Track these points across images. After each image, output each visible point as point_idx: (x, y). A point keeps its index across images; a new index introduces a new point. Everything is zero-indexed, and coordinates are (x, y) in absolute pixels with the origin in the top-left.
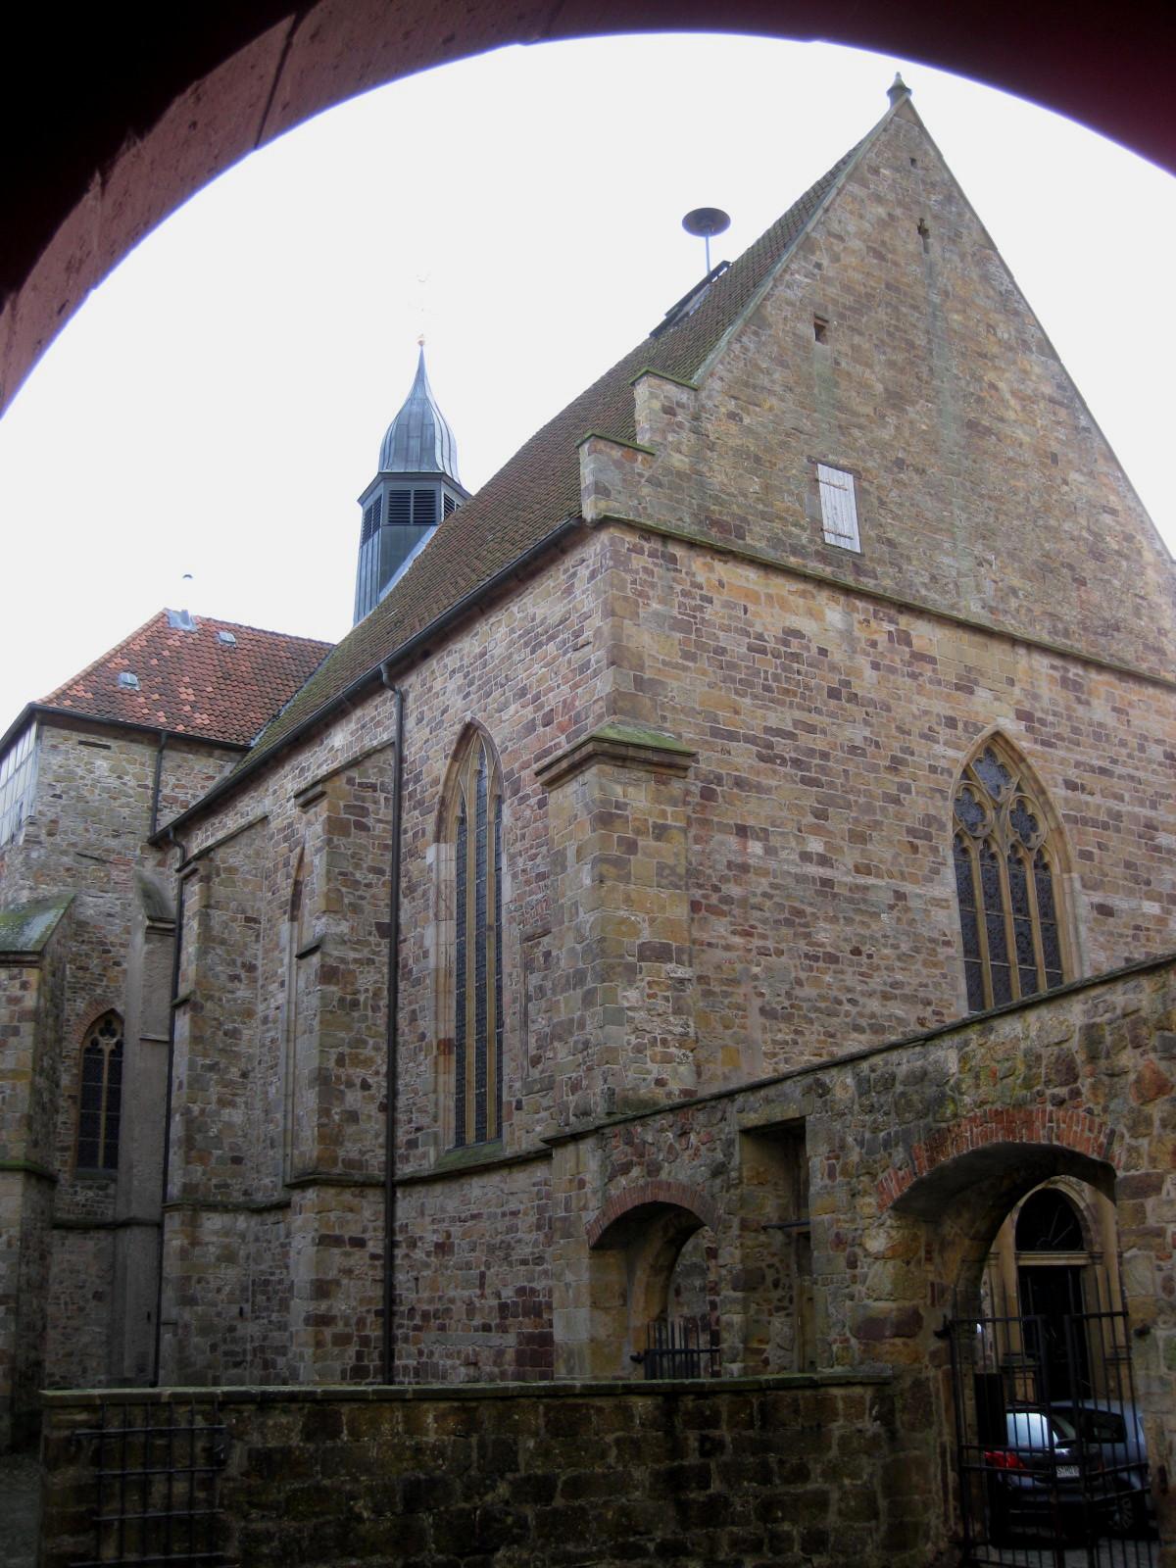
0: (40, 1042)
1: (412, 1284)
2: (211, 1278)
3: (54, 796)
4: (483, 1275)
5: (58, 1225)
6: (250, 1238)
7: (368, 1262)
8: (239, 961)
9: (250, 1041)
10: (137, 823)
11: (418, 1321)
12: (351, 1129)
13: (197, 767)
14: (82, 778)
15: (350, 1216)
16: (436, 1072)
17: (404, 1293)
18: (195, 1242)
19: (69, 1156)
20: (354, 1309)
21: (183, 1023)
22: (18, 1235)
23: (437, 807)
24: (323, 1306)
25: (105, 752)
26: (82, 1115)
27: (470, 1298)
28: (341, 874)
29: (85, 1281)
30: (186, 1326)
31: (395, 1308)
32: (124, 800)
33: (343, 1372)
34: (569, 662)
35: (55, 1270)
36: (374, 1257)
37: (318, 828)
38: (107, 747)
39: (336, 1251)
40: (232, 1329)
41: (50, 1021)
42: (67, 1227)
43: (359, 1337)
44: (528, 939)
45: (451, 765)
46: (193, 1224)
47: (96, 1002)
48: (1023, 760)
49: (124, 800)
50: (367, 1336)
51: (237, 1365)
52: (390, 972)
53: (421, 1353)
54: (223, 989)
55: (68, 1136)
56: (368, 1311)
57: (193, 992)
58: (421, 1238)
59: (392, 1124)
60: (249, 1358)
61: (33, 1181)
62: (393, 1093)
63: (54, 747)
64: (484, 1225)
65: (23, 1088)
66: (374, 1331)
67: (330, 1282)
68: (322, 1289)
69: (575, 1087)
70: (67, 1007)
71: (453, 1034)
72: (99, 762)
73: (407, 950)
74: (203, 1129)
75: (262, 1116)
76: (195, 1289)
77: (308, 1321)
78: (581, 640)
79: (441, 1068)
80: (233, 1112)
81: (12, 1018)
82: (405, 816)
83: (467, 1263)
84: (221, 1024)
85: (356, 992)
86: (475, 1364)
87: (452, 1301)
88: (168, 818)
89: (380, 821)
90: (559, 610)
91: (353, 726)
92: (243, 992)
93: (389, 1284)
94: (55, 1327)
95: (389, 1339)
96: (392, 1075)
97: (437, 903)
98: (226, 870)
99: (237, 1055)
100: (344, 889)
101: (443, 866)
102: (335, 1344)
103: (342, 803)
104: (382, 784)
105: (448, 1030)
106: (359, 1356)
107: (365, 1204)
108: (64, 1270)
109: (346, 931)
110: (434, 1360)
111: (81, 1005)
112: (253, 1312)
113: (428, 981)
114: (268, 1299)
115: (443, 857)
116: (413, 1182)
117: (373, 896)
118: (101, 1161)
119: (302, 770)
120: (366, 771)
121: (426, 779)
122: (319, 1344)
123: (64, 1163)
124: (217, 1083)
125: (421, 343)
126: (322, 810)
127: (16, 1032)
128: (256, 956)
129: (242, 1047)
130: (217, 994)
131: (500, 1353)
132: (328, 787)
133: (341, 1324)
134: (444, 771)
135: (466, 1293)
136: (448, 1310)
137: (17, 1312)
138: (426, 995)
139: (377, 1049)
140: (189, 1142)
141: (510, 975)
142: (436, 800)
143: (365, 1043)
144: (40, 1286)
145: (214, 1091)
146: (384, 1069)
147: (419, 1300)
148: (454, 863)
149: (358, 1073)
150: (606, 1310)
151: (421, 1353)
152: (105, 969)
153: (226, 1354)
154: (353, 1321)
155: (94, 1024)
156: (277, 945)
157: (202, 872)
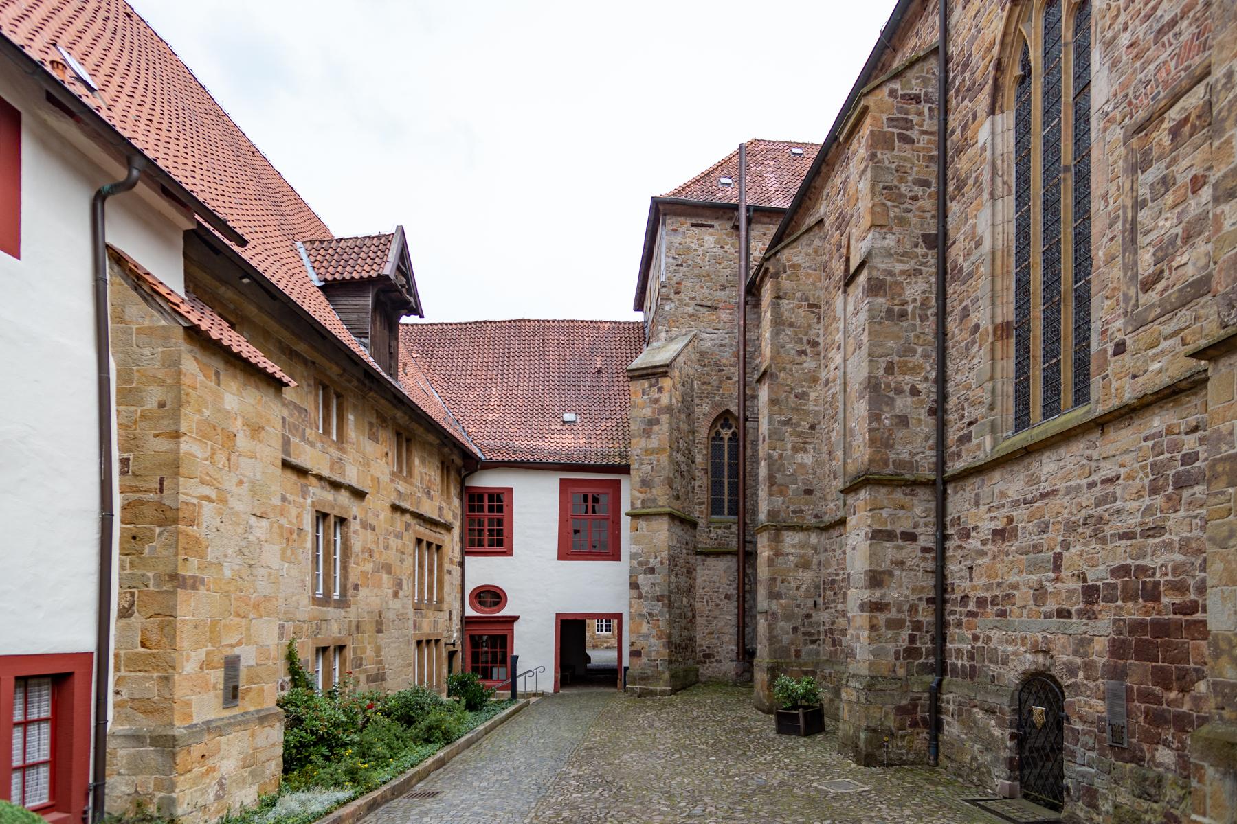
1: (966, 573)
2: (791, 579)
4: (1058, 558)
6: (821, 549)
7: (920, 554)
9: (816, 401)
11: (972, 607)
12: (901, 433)
14: (696, 250)
15: (901, 512)
17: (957, 583)
18: (778, 554)
20: (907, 596)
21: (764, 393)
24: (877, 594)
25: (710, 230)
27: (1040, 583)
30: (774, 614)
31: (947, 596)
33: (897, 653)
35: (699, 581)
36: (925, 550)
38: (712, 226)
39: (888, 544)
40: (809, 616)
41: (683, 416)
42: (708, 554)
43: (911, 622)
46: (776, 540)
47: (715, 405)
50: (919, 622)
52: (937, 283)
53: (976, 638)
54: (793, 362)
55: (703, 495)
56: (920, 599)
57: (770, 366)
58: (975, 528)
59: (942, 427)
60: (822, 637)
62: (943, 397)
63: (675, 230)
64: (1054, 503)
65: (664, 459)
66: (926, 616)
67: (883, 573)
68: (876, 579)
70: (697, 410)
71: (1012, 317)
72: (706, 238)
74: (782, 468)
76: (779, 587)
77: (862, 607)
79: (998, 355)
80: (805, 456)
83: (1035, 546)
84: (792, 389)
85: (904, 303)
86: (1046, 652)
87: (1015, 586)
92: (809, 363)
93: (940, 575)
95: (942, 624)
96: (942, 380)
97: (993, 180)
98: (790, 266)
99: (807, 412)
100: (889, 203)
101: (999, 140)
103: (885, 117)
104: (926, 94)
105: (1007, 312)
106: (912, 639)
107: (916, 502)
109: (892, 244)
110: (992, 645)
111: (706, 408)
115: (999, 129)
120: (909, 82)
122: (873, 628)
123: (701, 512)
124: (791, 434)
127: (657, 422)
129: (811, 406)
130: (788, 366)
131: (1083, 643)
136: (1009, 596)
137: (670, 606)
138: (981, 286)
139: (926, 356)
140: (771, 478)
141: (1105, 197)
143: (915, 352)
144: (690, 591)
145: (789, 441)
146: (933, 375)
147: (974, 588)
149: (908, 380)
151: (976, 638)
152: (721, 382)
153: (805, 634)
154: (906, 607)
155: (715, 421)
157: (772, 270)
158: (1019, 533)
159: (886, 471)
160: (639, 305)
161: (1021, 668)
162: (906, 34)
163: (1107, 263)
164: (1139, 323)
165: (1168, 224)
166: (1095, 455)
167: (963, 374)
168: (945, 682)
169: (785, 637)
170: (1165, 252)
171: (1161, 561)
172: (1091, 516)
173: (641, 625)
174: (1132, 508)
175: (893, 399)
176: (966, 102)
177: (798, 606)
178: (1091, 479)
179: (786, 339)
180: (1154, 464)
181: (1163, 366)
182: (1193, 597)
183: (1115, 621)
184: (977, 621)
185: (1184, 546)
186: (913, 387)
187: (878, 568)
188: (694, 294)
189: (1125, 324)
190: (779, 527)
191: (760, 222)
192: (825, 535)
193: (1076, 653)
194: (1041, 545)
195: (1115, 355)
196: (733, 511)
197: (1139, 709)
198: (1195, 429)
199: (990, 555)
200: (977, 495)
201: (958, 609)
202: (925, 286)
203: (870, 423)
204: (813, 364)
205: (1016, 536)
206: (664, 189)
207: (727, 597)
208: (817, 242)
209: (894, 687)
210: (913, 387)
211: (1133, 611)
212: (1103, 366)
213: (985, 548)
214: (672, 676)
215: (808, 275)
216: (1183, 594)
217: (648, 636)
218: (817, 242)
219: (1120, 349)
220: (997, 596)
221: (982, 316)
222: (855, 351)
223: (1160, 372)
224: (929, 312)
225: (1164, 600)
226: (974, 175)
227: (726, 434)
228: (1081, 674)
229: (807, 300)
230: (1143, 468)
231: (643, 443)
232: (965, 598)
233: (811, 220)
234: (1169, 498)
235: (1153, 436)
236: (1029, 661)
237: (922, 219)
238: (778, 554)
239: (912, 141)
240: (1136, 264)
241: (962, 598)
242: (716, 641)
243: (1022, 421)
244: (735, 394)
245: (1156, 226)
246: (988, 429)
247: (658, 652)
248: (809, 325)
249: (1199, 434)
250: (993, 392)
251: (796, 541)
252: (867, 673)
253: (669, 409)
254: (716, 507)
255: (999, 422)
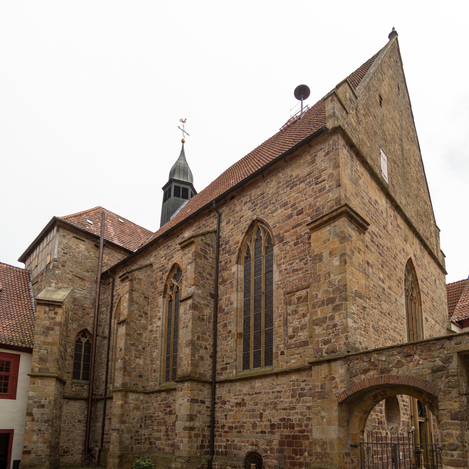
0: (62, 334)
1: (224, 417)
2: (131, 415)
3: (64, 253)
4: (261, 414)
5: (65, 398)
6: (144, 402)
8: (142, 311)
9: (145, 337)
10: (95, 269)
12: (201, 363)
13: (115, 255)
14: (74, 249)
15: (200, 392)
16: (236, 344)
17: (220, 420)
18: (126, 403)
19: (70, 375)
20: (201, 425)
22: (53, 399)
23: (237, 252)
25: (83, 242)
26: (75, 362)
28: (199, 272)
29: (75, 416)
30: (122, 431)
31: (215, 425)
32: (90, 260)
33: (197, 447)
34: (313, 189)
35: (64, 412)
36: (207, 407)
37: (190, 255)
38: (84, 241)
39: (196, 404)
41: (65, 328)
42: (70, 399)
43: (202, 435)
44: (288, 293)
45: (245, 236)
46: (125, 396)
47: (79, 326)
48: (414, 269)
49: (90, 260)
51: (139, 443)
54: (137, 319)
55: (71, 370)
56: (205, 426)
58: (228, 401)
60: (143, 441)
61: (58, 382)
62: (215, 352)
64: (260, 396)
65: (55, 349)
66: (207, 433)
67: (194, 415)
68: (191, 418)
69: (326, 342)
70: (70, 326)
71: (242, 332)
72: (81, 245)
73: (223, 303)
74: (129, 365)
75: (150, 362)
76: (125, 418)
78: (319, 180)
80: (140, 360)
81: (51, 324)
82: (220, 257)
83: (253, 410)
84: (136, 331)
86: (256, 445)
87: (245, 423)
88: (105, 269)
89: (211, 258)
90: (307, 170)
91: (194, 228)
92: (143, 321)
94: (64, 431)
96: (215, 345)
97: (237, 285)
98: (138, 279)
99: (141, 342)
100: (200, 278)
101: (239, 273)
102: (195, 437)
103: (199, 247)
105: (241, 329)
106: (202, 441)
108: (67, 413)
110: (235, 443)
111: (75, 326)
112: (145, 426)
113: (233, 313)
114: (152, 422)
115: (239, 270)
116: (223, 382)
117: (209, 283)
118: (81, 378)
119: (169, 247)
121: (231, 243)
122: (190, 437)
123: (68, 377)
125: (183, 142)
126: (193, 248)
128: (148, 310)
129: (143, 340)
130: (135, 320)
131: (270, 442)
132: (195, 240)
133: (197, 430)
134: (242, 238)
135: (252, 420)
136: (242, 426)
137: (52, 426)
138: (232, 317)
140: (124, 369)
141: (278, 307)
142: (237, 249)
143: (206, 334)
144: (59, 418)
145: (134, 353)
146: (212, 343)
147: (227, 423)
148: (243, 272)
149: (204, 343)
150: (343, 426)
151: (228, 441)
152: (84, 315)
153: (135, 440)
154: (201, 429)
155: (79, 333)
156: (157, 306)
157: (130, 278)
158: (247, 405)
159: (196, 376)
160: (23, 259)
161: (246, 451)
162: (201, 218)
163: (278, 327)
164: (288, 347)
165: (296, 323)
166: (274, 383)
167: (224, 346)
168: (213, 458)
169: (127, 441)
170: (296, 330)
171: (295, 418)
172: (273, 402)
173: (32, 436)
174: (286, 401)
175: (199, 350)
176: (227, 255)
177: (133, 427)
178: (273, 390)
179: (134, 308)
180: (293, 389)
181: (294, 362)
182: (304, 428)
183: (281, 435)
184: (228, 434)
185: (301, 413)
186: (205, 346)
187: (192, 414)
188: (72, 270)
189: (284, 347)
190: (126, 390)
191: (108, 247)
192: (146, 396)
193: (267, 445)
194: (255, 409)
195: (281, 354)
196: (86, 377)
197: (288, 462)
198: (304, 381)
199: (235, 411)
200: (229, 389)
201: (220, 430)
202: (210, 311)
203: (191, 357)
204: (145, 322)
205: (245, 405)
206: (60, 215)
207: (79, 421)
208: (149, 272)
209: (196, 460)
210: (205, 346)
211: (286, 432)
212: (277, 357)
213: (232, 409)
214: (51, 464)
215: (145, 285)
216: (301, 427)
217: (36, 442)
218: (149, 272)
219: (282, 353)
220: (237, 426)
221: (232, 328)
222: (184, 327)
223: (294, 363)
224: (211, 321)
225: (296, 429)
226: (230, 280)
227: (84, 340)
228: (269, 452)
229: (144, 294)
230: (290, 390)
231: (42, 338)
232: (223, 426)
233: (148, 262)
234: (297, 400)
235: (292, 381)
236: (250, 448)
237: (210, 288)
238: (126, 403)
239: (207, 259)
240: (287, 331)
241: (222, 426)
242: (71, 444)
243: (246, 366)
244: (91, 322)
245: (293, 322)
246: (234, 367)
247: (43, 451)
248: (144, 305)
249: (305, 383)
250: (236, 355)
251: (134, 398)
252: (187, 455)
253: (60, 324)
254: (76, 375)
255: (238, 365)
